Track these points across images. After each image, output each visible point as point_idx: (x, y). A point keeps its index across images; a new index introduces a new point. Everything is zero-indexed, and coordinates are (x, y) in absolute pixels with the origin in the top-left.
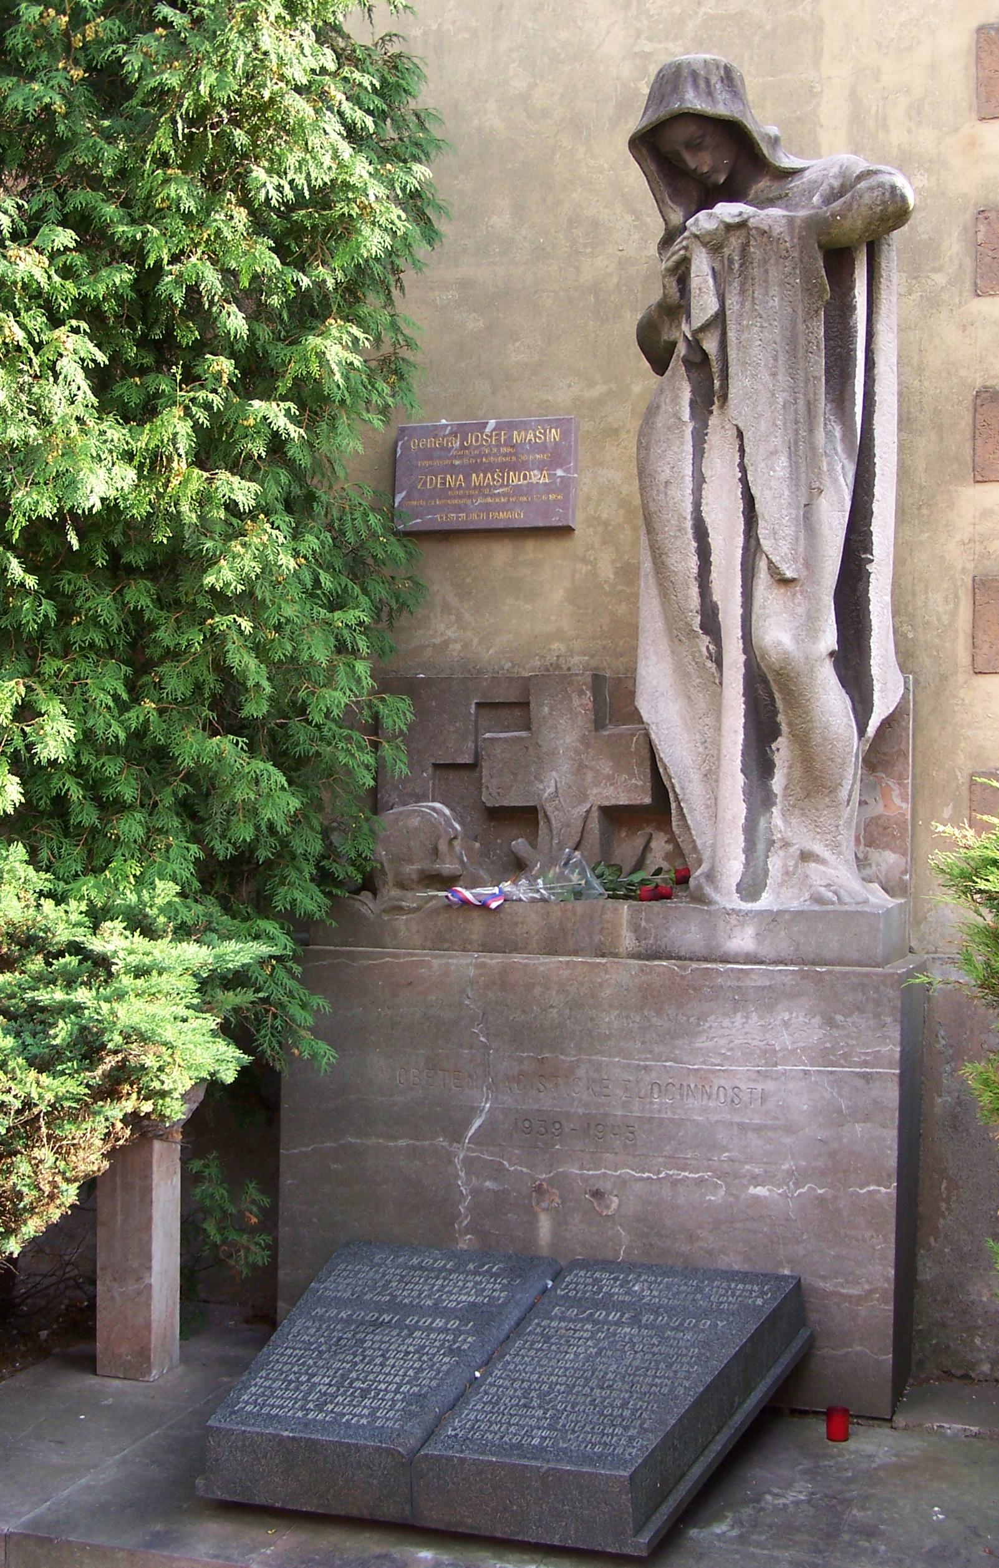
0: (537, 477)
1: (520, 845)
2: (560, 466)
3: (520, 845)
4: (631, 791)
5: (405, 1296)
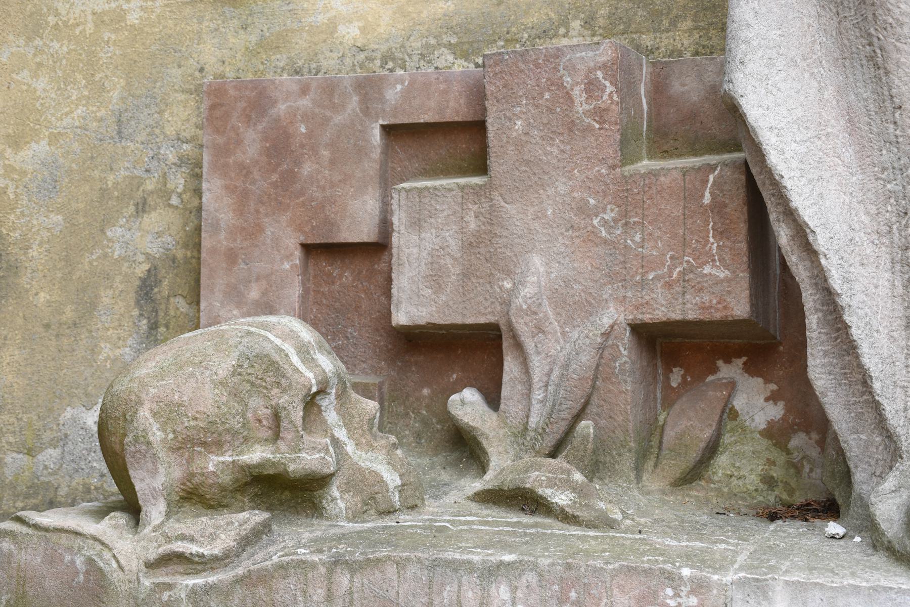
1: (467, 405)
3: (467, 405)
4: (718, 289)
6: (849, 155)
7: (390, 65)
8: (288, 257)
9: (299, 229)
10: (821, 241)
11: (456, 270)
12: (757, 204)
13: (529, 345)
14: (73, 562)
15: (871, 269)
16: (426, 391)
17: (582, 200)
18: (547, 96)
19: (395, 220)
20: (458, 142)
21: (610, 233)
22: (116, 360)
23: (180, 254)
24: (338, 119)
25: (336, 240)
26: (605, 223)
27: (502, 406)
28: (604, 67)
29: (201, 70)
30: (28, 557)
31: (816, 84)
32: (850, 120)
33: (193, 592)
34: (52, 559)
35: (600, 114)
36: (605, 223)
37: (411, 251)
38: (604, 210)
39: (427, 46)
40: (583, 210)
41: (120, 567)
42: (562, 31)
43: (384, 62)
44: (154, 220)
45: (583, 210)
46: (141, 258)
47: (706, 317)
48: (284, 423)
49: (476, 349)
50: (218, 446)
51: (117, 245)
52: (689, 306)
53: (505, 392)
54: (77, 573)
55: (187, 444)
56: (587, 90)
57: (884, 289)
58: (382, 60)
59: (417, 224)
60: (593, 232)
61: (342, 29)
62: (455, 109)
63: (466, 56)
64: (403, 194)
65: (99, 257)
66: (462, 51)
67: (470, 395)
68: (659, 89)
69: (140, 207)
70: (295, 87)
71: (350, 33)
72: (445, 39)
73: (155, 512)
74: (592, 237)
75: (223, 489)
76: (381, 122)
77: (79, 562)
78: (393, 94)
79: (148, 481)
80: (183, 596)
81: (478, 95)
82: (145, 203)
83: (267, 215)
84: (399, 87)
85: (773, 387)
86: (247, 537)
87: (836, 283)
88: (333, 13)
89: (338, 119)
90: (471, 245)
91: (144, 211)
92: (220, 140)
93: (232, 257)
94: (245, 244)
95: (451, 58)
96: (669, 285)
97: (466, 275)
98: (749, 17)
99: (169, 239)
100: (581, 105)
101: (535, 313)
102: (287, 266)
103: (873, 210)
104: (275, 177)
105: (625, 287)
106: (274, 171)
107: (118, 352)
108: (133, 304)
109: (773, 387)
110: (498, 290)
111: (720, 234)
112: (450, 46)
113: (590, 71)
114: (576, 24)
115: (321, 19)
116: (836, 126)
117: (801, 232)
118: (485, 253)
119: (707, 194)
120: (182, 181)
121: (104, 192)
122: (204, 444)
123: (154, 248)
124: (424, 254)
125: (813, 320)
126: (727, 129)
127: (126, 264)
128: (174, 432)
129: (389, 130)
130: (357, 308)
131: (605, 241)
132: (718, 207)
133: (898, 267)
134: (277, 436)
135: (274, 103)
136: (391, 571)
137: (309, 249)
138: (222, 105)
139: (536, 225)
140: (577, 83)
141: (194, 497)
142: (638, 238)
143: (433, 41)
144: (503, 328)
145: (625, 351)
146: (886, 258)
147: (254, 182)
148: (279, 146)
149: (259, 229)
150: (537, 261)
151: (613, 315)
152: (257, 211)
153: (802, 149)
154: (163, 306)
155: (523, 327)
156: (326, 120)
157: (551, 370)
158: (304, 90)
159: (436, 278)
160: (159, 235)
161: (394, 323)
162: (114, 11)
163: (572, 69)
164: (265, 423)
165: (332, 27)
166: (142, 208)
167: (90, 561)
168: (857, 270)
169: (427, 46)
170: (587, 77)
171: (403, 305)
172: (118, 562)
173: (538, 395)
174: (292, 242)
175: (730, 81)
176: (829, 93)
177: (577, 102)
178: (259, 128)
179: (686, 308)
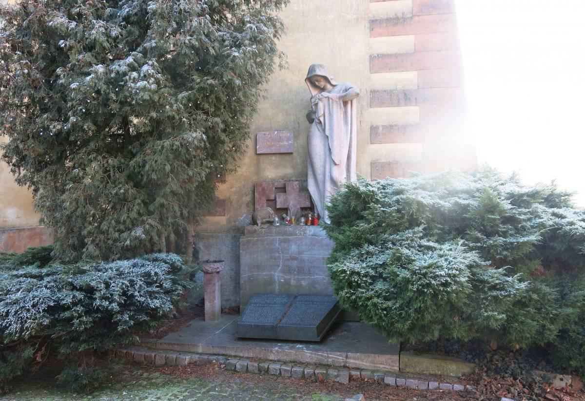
0: (286, 143)
1: (284, 215)
3: (284, 215)
5: (268, 302)
20: (283, 189)
49: (286, 210)
59: (279, 198)
62: (282, 186)
66: (283, 179)
71: (270, 177)
73: (259, 225)
78: (276, 184)
81: (285, 184)
90: (284, 200)
118: (286, 201)
137: (267, 200)
141: (262, 223)
148: (263, 189)
151: (298, 207)
159: (281, 203)
165: (33, 392)
166: (246, 196)
174: (265, 199)
179: (305, 206)
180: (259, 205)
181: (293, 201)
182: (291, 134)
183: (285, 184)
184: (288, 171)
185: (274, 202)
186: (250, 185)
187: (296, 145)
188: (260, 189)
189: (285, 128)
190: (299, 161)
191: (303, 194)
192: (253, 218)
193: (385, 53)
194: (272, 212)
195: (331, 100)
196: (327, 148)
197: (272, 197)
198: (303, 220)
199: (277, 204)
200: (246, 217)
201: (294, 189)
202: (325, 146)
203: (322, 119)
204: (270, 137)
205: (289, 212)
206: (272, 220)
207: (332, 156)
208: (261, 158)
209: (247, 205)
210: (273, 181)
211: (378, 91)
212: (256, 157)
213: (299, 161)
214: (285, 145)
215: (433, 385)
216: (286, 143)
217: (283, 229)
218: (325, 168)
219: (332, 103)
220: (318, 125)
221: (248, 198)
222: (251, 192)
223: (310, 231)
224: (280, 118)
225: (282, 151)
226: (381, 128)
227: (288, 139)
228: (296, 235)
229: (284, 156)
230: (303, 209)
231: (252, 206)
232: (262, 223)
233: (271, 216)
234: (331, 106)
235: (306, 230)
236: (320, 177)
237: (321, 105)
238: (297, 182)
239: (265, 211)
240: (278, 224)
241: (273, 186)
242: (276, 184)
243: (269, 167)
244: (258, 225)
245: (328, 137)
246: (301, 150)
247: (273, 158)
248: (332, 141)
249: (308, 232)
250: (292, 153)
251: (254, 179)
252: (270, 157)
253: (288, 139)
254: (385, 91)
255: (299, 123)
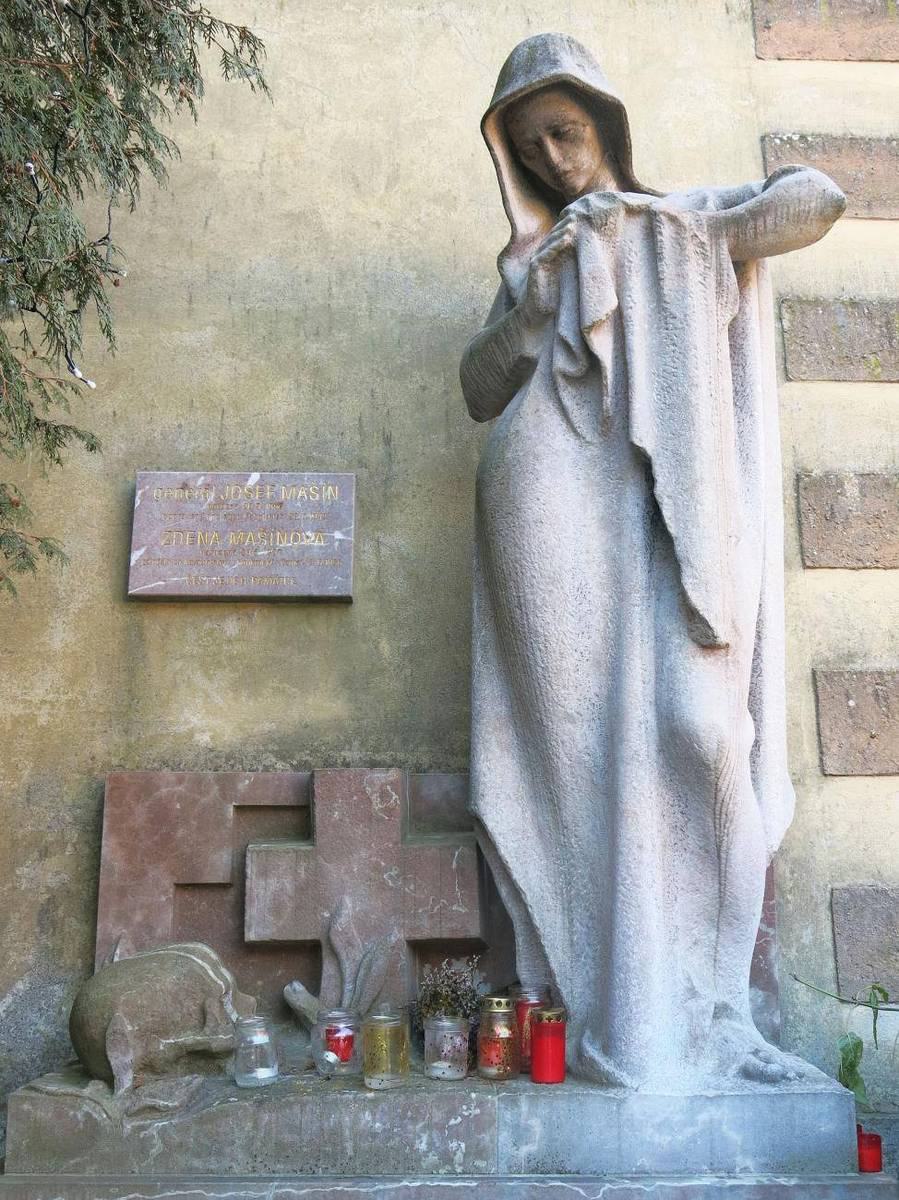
0: (311, 539)
1: (297, 993)
2: (340, 528)
3: (297, 993)
4: (462, 918)
6: (539, 849)
7: (232, 762)
8: (165, 892)
9: (173, 873)
10: (529, 899)
11: (290, 905)
12: (487, 873)
13: (343, 956)
14: (75, 1116)
15: (552, 912)
16: (260, 983)
17: (377, 862)
18: (355, 798)
19: (249, 871)
20: (297, 818)
21: (394, 883)
22: (22, 963)
23: (73, 887)
24: (204, 800)
25: (196, 882)
26: (391, 877)
27: (322, 994)
28: (391, 783)
29: (93, 758)
30: (43, 1114)
31: (520, 809)
32: (540, 831)
33: (163, 1131)
34: (60, 1115)
35: (389, 811)
36: (391, 877)
37: (261, 891)
38: (391, 870)
39: (258, 751)
40: (377, 868)
41: (109, 1117)
42: (347, 747)
43: (228, 759)
44: (53, 863)
45: (377, 868)
46: (43, 890)
47: (455, 936)
48: (208, 1017)
49: (307, 955)
50: (166, 1034)
51: (24, 880)
52: (443, 929)
53: (324, 984)
54: (78, 1122)
55: (148, 1034)
56: (381, 797)
57: (529, 898)
58: (226, 758)
59: (264, 873)
60: (384, 882)
61: (197, 737)
62: (286, 798)
63: (283, 758)
64: (255, 855)
65: (9, 889)
66: (282, 756)
67: (298, 986)
68: (415, 794)
69: (43, 853)
70: (173, 778)
71: (204, 739)
72: (270, 747)
73: (126, 1080)
74: (382, 886)
75: (167, 1061)
76: (234, 804)
77: (80, 1116)
78: (243, 785)
79: (121, 1058)
80: (155, 1133)
81: (307, 790)
82: (46, 849)
83: (150, 863)
84: (247, 782)
85: (484, 974)
86: (192, 1093)
87: (537, 922)
88: (192, 725)
89: (204, 800)
90: (301, 889)
91: (46, 856)
92: (117, 812)
93: (122, 892)
94: (133, 883)
95: (274, 760)
96: (432, 917)
97: (298, 908)
98: (484, 769)
99: (66, 876)
100: (377, 805)
101: (347, 934)
102: (163, 899)
103: (553, 880)
104: (156, 838)
105: (403, 917)
106: (156, 834)
107: (23, 958)
108: (35, 923)
109: (484, 974)
110: (320, 918)
111: (462, 886)
112: (272, 752)
113: (382, 785)
114: (356, 743)
115: (183, 729)
116: (532, 832)
117: (517, 893)
118: (312, 892)
119: (454, 863)
120: (76, 835)
121: (14, 843)
122: (156, 1032)
123: (51, 881)
124: (269, 893)
125: (520, 940)
126: (469, 825)
127: (31, 894)
128: (139, 1025)
129: (237, 808)
130: (211, 927)
131: (391, 888)
132: (461, 870)
133: (566, 912)
134: (203, 1022)
135: (158, 788)
136: (297, 1109)
137: (178, 886)
138: (119, 788)
139: (346, 878)
140: (375, 792)
142: (412, 887)
143: (261, 748)
144: (323, 943)
145: (405, 958)
146: (559, 907)
147: (141, 841)
148: (161, 817)
149: (145, 873)
150: (348, 901)
151: (398, 936)
152: (143, 861)
153: (516, 845)
154: (59, 925)
155: (337, 942)
156: (195, 801)
157: (359, 971)
158: (180, 781)
159: (277, 909)
160: (58, 873)
161: (246, 940)
162: (29, 715)
163: (371, 783)
164: (194, 1016)
165: (191, 734)
166: (45, 853)
167: (88, 1115)
168: (545, 914)
169: (258, 751)
170: (381, 789)
171: (253, 927)
172: (106, 1113)
173: (349, 987)
174: (168, 883)
175: (476, 805)
176: (528, 815)
177: (374, 804)
178: (147, 804)
179: (444, 932)
180: (123, 918)
181: (362, 899)
182: (344, 496)
183: (307, 790)
184: (320, 705)
185: (230, 896)
186: (72, 792)
187: (369, 559)
188: (140, 815)
189: (304, 457)
190: (385, 647)
191: (432, 846)
192: (77, 1025)
193: (839, 133)
194: (221, 976)
195: (666, 232)
196: (635, 534)
197: (218, 865)
198: (448, 1031)
199: (252, 912)
200: (29, 998)
201: (370, 818)
202: (613, 525)
203: (603, 345)
204: (219, 502)
205: (328, 969)
206: (222, 1040)
207: (688, 583)
208: (155, 623)
209: (46, 917)
210: (224, 764)
211: (816, 302)
212: (120, 618)
213: (385, 647)
214: (314, 547)
215: (182, 954)
216: (311, 539)
217: (307, 1116)
218: (614, 671)
219: (680, 245)
220: (568, 396)
221: (52, 873)
222: (73, 835)
223: (520, 1135)
224: (281, 404)
225: (290, 584)
226: (852, 490)
227: (329, 519)
228: (409, 1164)
229: (293, 616)
230: (424, 950)
231: (74, 925)
232: (149, 1067)
233: (213, 1009)
234: (668, 268)
235: (479, 1124)
236: (574, 738)
237: (597, 255)
238: (393, 774)
239: (166, 976)
240: (264, 1074)
241: (225, 796)
242: (243, 785)
243: (198, 678)
244: (110, 1081)
245: (643, 465)
246: (397, 586)
247: (231, 625)
248: (688, 489)
249: (504, 1137)
250: (345, 601)
251: (99, 746)
252: (205, 622)
253: (329, 519)
254: (854, 304)
255: (388, 441)
